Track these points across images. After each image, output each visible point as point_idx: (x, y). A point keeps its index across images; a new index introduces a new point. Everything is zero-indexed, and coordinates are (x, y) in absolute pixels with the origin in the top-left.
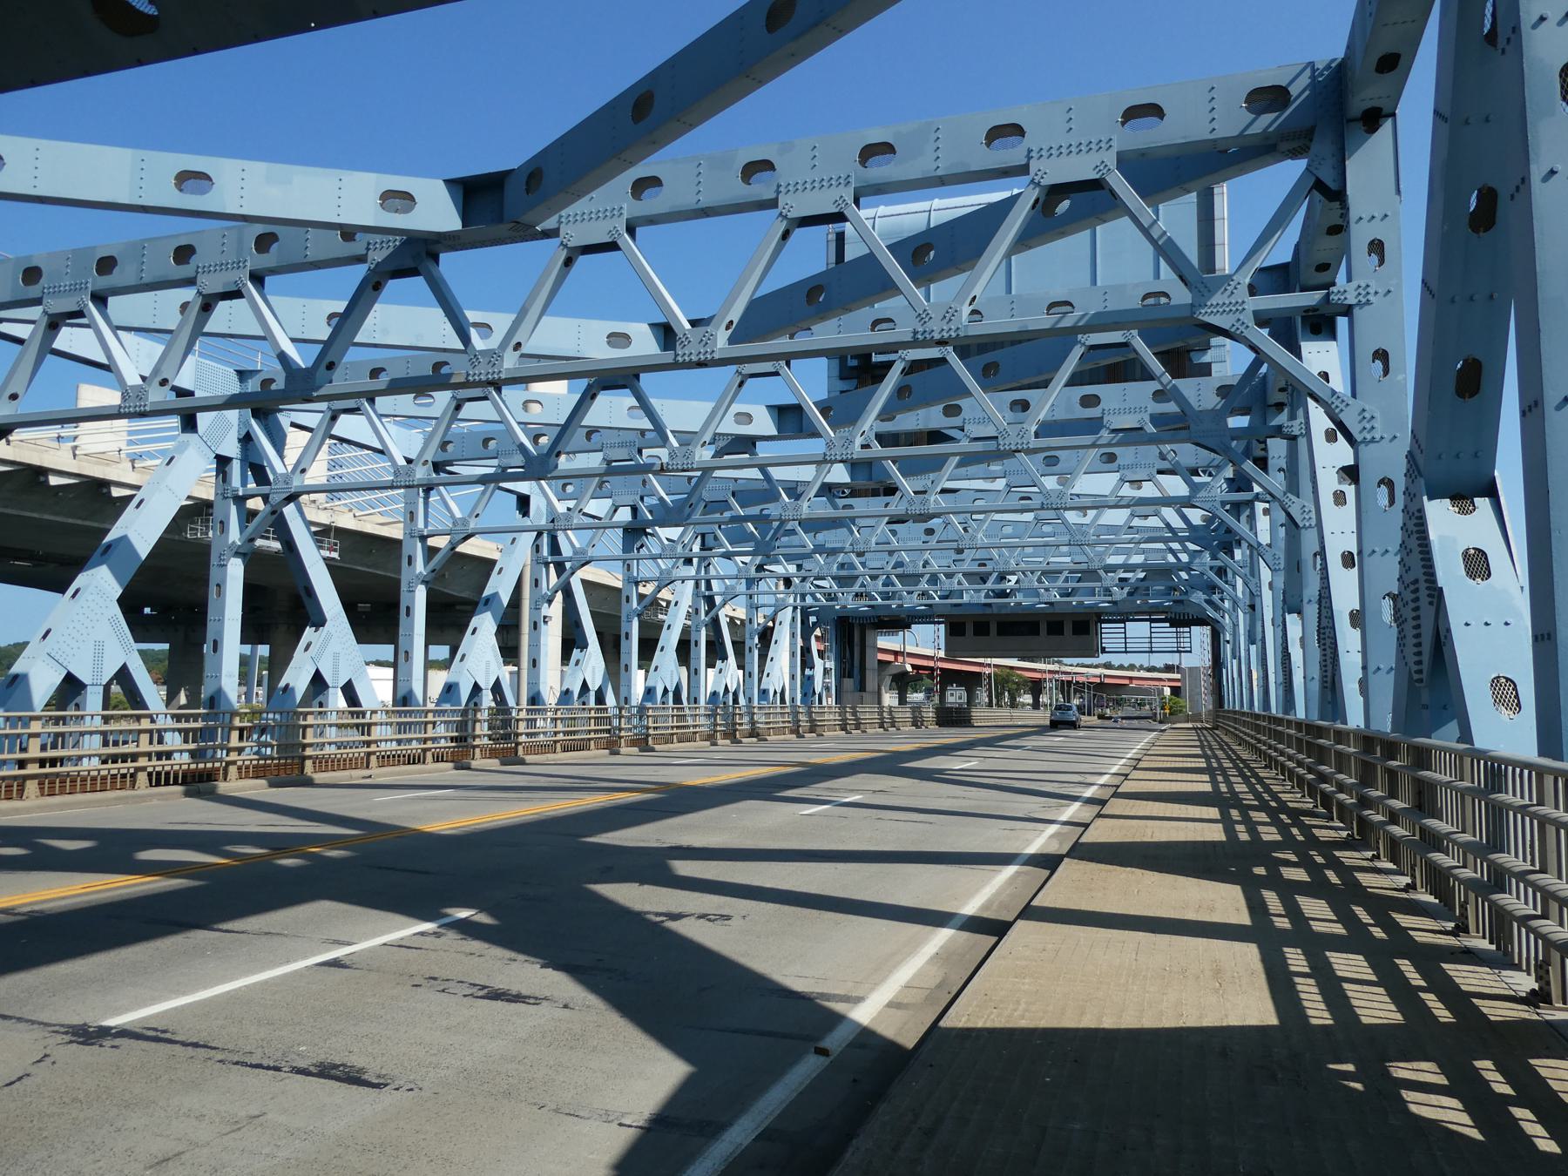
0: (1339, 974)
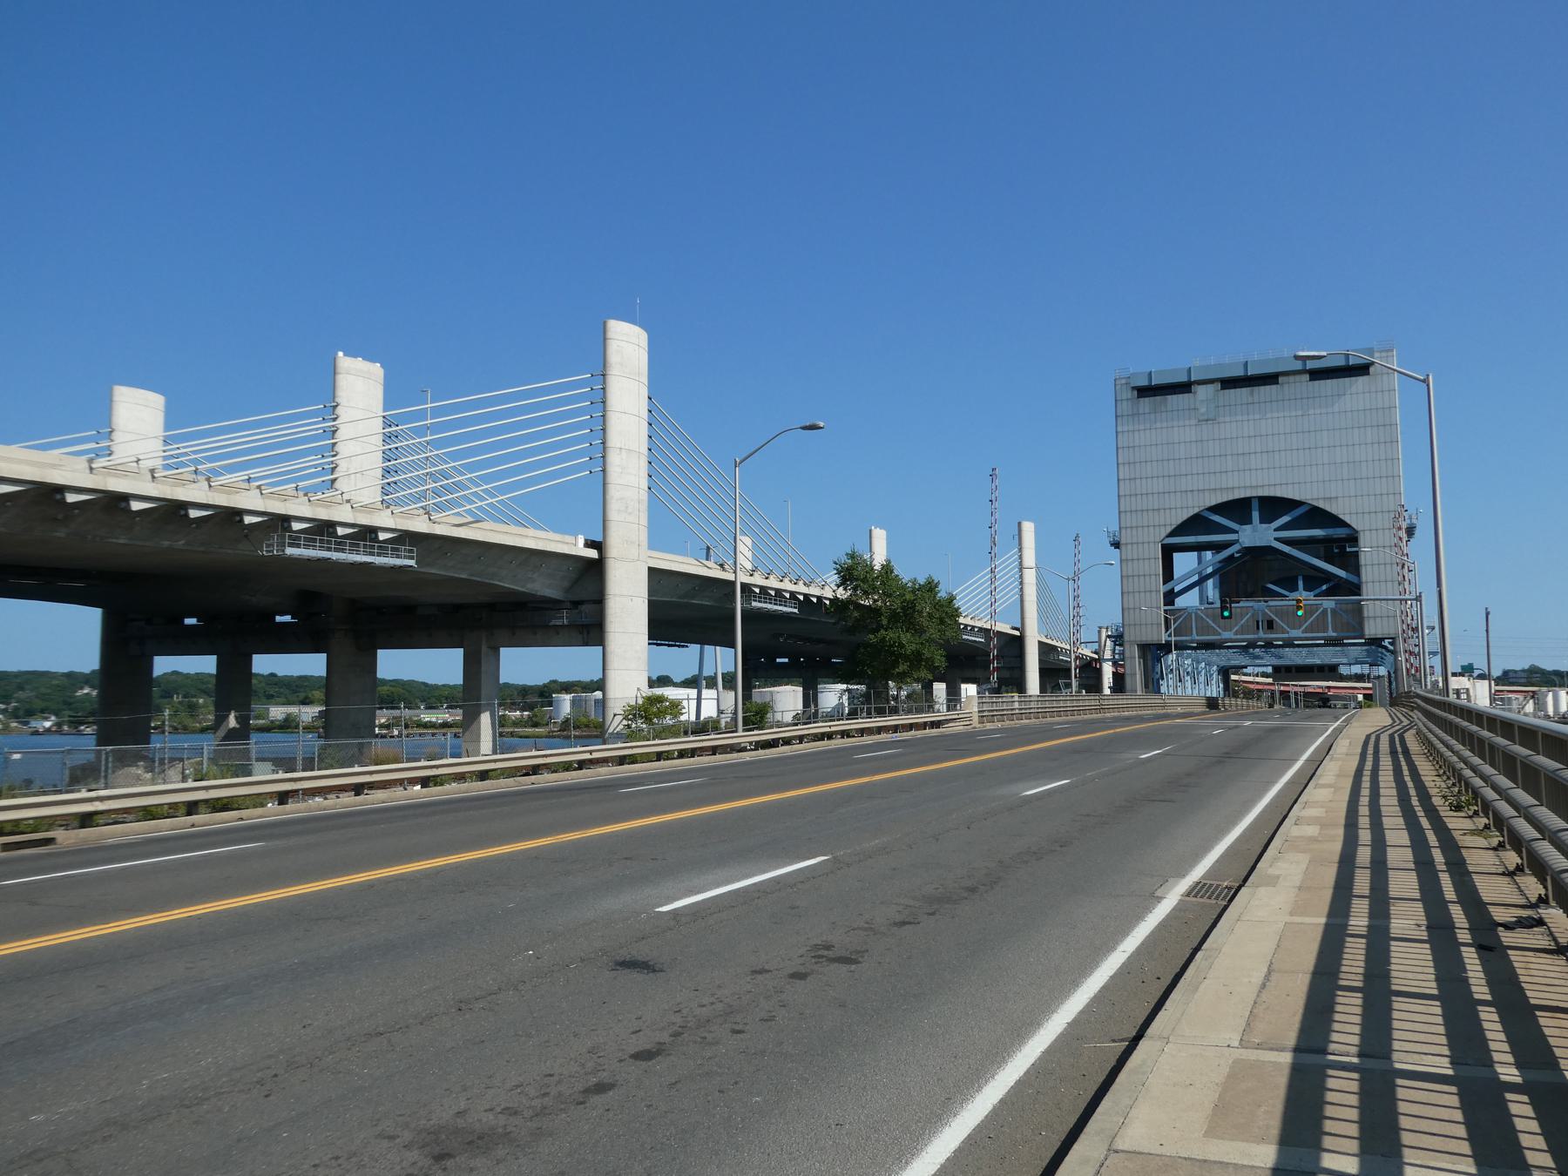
0: (1533, 1001)
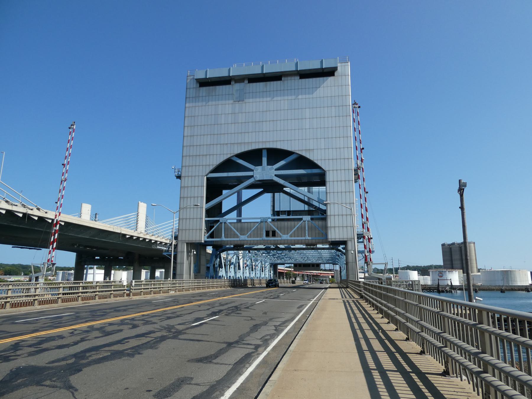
0: (369, 338)
